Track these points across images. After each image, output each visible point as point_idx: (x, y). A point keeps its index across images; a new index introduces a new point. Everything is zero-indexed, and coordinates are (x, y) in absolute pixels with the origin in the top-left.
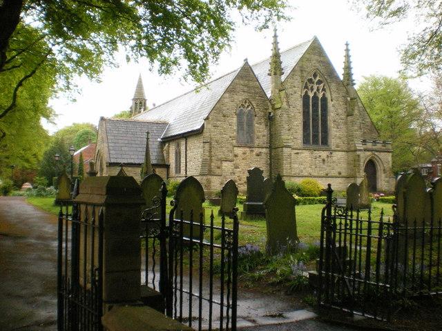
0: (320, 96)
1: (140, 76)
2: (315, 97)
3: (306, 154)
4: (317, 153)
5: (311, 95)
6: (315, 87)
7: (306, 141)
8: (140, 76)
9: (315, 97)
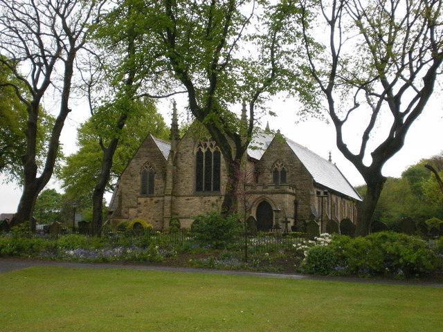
0: (212, 151)
2: (208, 152)
3: (197, 199)
4: (206, 198)
5: (204, 150)
6: (208, 144)
7: (198, 188)
9: (208, 152)
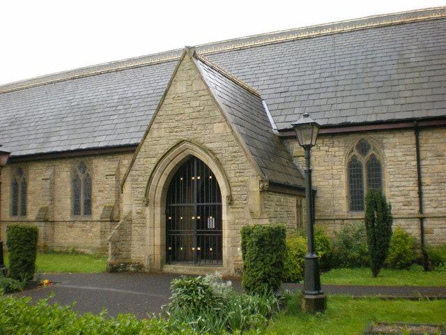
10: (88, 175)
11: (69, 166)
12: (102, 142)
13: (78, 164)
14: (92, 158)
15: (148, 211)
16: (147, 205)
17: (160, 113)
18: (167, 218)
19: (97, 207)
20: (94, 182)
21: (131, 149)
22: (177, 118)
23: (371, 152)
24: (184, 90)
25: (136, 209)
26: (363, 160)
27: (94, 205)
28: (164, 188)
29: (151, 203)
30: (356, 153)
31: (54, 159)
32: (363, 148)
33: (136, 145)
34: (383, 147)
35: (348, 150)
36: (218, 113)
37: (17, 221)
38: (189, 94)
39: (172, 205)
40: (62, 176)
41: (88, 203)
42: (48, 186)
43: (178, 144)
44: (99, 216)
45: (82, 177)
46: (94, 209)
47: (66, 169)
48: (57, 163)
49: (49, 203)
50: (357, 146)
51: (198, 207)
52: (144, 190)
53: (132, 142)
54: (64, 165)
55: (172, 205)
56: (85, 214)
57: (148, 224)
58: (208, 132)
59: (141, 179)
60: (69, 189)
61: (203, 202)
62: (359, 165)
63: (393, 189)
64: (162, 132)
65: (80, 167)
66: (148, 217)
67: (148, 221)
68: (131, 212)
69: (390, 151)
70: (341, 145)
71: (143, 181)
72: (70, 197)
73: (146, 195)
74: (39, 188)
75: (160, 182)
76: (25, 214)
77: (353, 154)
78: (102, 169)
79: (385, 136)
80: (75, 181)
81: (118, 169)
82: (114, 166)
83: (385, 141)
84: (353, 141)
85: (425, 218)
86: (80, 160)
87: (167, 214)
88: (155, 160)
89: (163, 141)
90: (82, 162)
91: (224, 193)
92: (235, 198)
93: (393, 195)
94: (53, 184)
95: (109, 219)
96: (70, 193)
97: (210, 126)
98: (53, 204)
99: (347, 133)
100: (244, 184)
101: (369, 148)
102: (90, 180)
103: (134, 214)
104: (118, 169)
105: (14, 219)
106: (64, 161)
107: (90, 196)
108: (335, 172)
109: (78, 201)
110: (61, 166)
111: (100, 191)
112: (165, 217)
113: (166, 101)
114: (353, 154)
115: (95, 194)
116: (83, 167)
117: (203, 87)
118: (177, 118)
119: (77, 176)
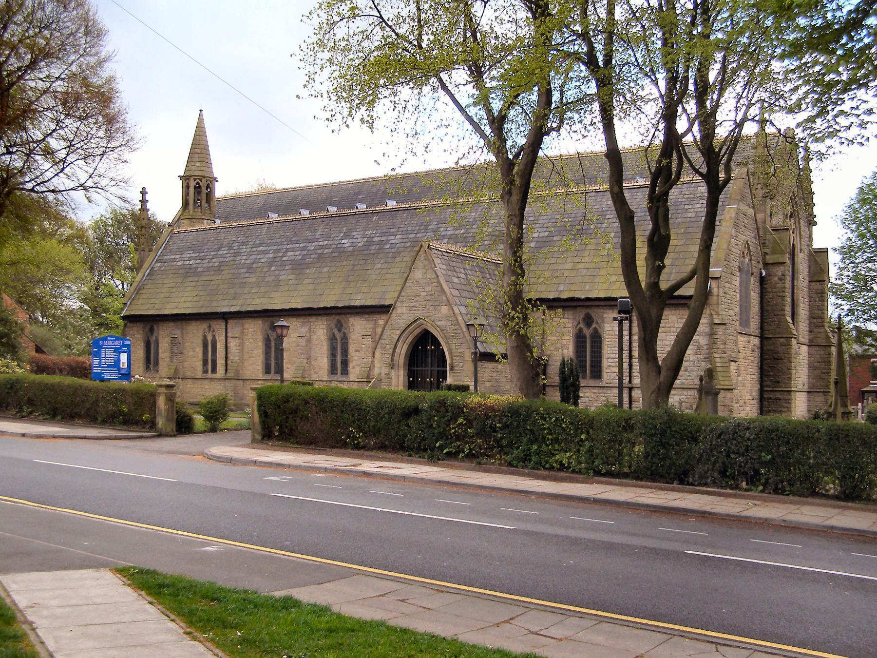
1: (201, 120)
8: (201, 120)
10: (345, 334)
11: (325, 323)
12: (358, 301)
13: (335, 321)
14: (349, 316)
15: (393, 373)
16: (392, 368)
17: (403, 294)
18: (409, 379)
19: (354, 367)
20: (350, 341)
21: (384, 309)
22: (415, 299)
23: (594, 325)
24: (420, 276)
25: (384, 371)
26: (587, 332)
27: (351, 365)
28: (406, 355)
29: (396, 367)
30: (582, 325)
31: (310, 315)
32: (588, 320)
33: (390, 306)
34: (603, 322)
35: (575, 323)
36: (444, 298)
37: (270, 382)
38: (424, 281)
39: (415, 369)
40: (318, 333)
41: (345, 363)
42: (304, 344)
43: (416, 321)
44: (355, 375)
45: (338, 336)
46: (350, 369)
47: (322, 326)
48: (313, 319)
49: (305, 361)
50: (584, 319)
51: (438, 371)
52: (390, 356)
53: (387, 303)
54: (320, 322)
55: (415, 369)
56: (342, 374)
57: (393, 384)
58: (437, 312)
59: (388, 347)
60: (325, 348)
61: (438, 367)
62: (585, 337)
63: (610, 360)
64: (404, 310)
65: (336, 326)
66: (393, 377)
67: (393, 381)
68: (380, 374)
69: (608, 325)
70: (570, 317)
71: (389, 348)
72: (326, 356)
73: (392, 360)
74: (294, 345)
75: (403, 350)
76: (347, 374)
77: (579, 326)
78: (358, 327)
79: (605, 311)
80: (332, 339)
81: (374, 329)
82: (370, 326)
83: (605, 316)
84: (581, 314)
85: (632, 387)
86: (337, 317)
87: (408, 375)
88: (398, 332)
89: (405, 317)
90: (339, 321)
91: (448, 361)
92: (455, 364)
93: (609, 366)
94: (309, 341)
95: (365, 380)
96: (326, 352)
97: (439, 308)
98: (310, 364)
99: (575, 307)
100: (461, 355)
101: (593, 321)
102: (347, 339)
103: (383, 374)
104: (374, 329)
105: (268, 377)
106: (320, 318)
107: (347, 356)
108: (564, 342)
109: (335, 360)
110: (316, 323)
111: (357, 351)
112: (407, 378)
113: (407, 284)
114: (578, 327)
115: (352, 354)
116: (340, 326)
117: (434, 276)
118: (415, 299)
119: (334, 334)
